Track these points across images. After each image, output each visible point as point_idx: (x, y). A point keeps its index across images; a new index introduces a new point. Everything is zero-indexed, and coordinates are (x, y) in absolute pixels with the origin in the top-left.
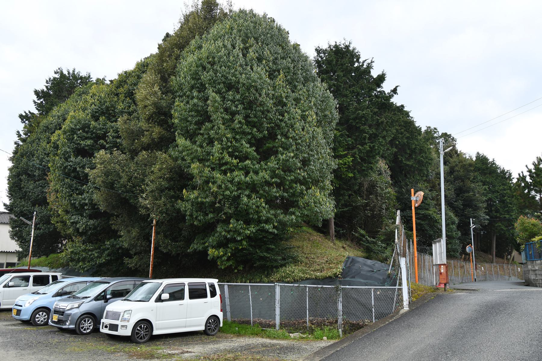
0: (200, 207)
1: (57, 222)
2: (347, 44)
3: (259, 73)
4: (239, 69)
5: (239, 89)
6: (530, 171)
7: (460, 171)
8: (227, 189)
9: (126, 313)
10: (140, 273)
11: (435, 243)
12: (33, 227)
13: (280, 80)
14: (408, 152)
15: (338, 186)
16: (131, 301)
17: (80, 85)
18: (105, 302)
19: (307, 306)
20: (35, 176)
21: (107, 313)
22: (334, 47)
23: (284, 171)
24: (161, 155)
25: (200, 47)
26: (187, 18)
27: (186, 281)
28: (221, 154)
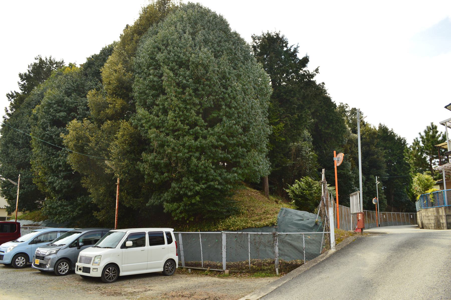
0: (156, 167)
1: (38, 182)
2: (277, 32)
3: (204, 54)
4: (190, 49)
5: (188, 66)
6: (422, 137)
7: (366, 138)
8: (179, 151)
9: (96, 258)
10: (107, 226)
11: (352, 196)
12: (18, 187)
13: (224, 59)
14: (327, 122)
15: (272, 149)
16: (100, 247)
17: (55, 68)
18: (78, 249)
19: (249, 250)
20: (19, 144)
21: (80, 258)
22: (266, 35)
23: (228, 137)
24: (124, 124)
25: (157, 33)
26: (145, 11)
27: (147, 230)
28: (175, 121)
